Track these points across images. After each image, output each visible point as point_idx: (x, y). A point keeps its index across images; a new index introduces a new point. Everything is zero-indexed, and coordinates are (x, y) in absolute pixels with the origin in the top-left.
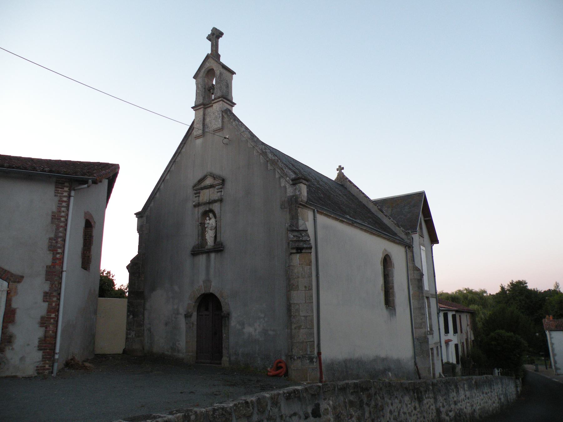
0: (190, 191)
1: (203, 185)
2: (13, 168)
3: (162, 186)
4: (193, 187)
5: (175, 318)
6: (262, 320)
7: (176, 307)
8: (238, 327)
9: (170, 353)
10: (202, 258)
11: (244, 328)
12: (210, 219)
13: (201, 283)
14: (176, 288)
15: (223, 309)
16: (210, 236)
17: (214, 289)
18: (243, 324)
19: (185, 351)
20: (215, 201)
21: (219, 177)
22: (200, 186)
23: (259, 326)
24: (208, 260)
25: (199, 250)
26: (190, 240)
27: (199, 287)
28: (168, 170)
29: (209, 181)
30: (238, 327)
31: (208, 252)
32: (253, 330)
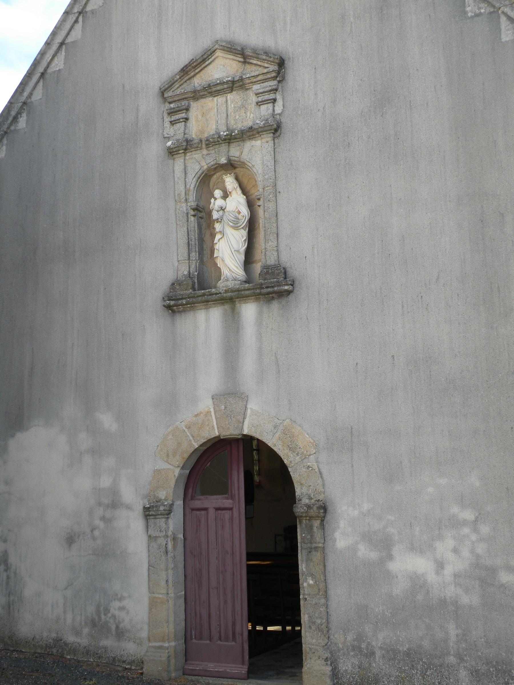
0: (150, 106)
1: (198, 81)
2: (184, 83)
3: (38, 94)
4: (162, 93)
5: (103, 518)
6: (466, 530)
7: (106, 482)
8: (364, 552)
9: (83, 641)
10: (207, 323)
11: (390, 557)
12: (226, 196)
13: (206, 404)
14: (107, 421)
15: (298, 491)
16: (228, 252)
17: (258, 420)
18: (385, 545)
19: (144, 634)
20: (250, 133)
21: (266, 53)
22: (188, 87)
23: (455, 551)
24: (233, 325)
25: (193, 291)
26: (165, 263)
27: (202, 418)
28: (59, 39)
29: (223, 68)
30: (364, 552)
31: (231, 299)
32: (431, 565)
